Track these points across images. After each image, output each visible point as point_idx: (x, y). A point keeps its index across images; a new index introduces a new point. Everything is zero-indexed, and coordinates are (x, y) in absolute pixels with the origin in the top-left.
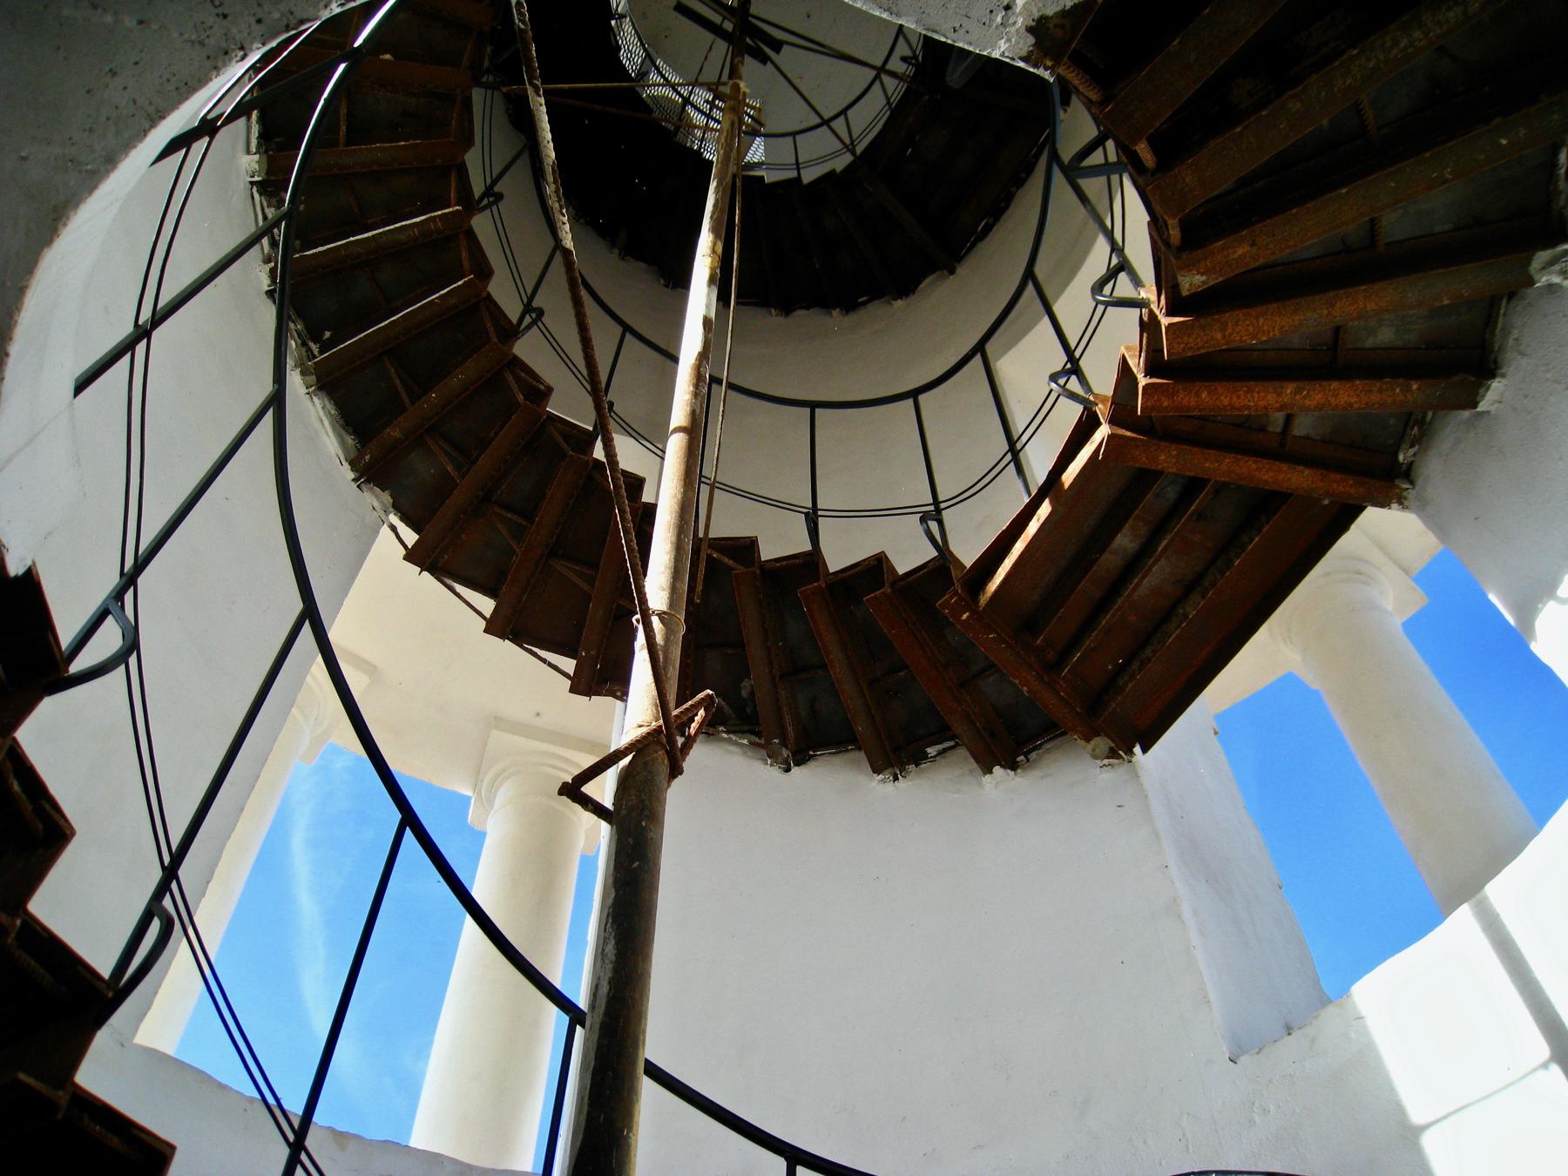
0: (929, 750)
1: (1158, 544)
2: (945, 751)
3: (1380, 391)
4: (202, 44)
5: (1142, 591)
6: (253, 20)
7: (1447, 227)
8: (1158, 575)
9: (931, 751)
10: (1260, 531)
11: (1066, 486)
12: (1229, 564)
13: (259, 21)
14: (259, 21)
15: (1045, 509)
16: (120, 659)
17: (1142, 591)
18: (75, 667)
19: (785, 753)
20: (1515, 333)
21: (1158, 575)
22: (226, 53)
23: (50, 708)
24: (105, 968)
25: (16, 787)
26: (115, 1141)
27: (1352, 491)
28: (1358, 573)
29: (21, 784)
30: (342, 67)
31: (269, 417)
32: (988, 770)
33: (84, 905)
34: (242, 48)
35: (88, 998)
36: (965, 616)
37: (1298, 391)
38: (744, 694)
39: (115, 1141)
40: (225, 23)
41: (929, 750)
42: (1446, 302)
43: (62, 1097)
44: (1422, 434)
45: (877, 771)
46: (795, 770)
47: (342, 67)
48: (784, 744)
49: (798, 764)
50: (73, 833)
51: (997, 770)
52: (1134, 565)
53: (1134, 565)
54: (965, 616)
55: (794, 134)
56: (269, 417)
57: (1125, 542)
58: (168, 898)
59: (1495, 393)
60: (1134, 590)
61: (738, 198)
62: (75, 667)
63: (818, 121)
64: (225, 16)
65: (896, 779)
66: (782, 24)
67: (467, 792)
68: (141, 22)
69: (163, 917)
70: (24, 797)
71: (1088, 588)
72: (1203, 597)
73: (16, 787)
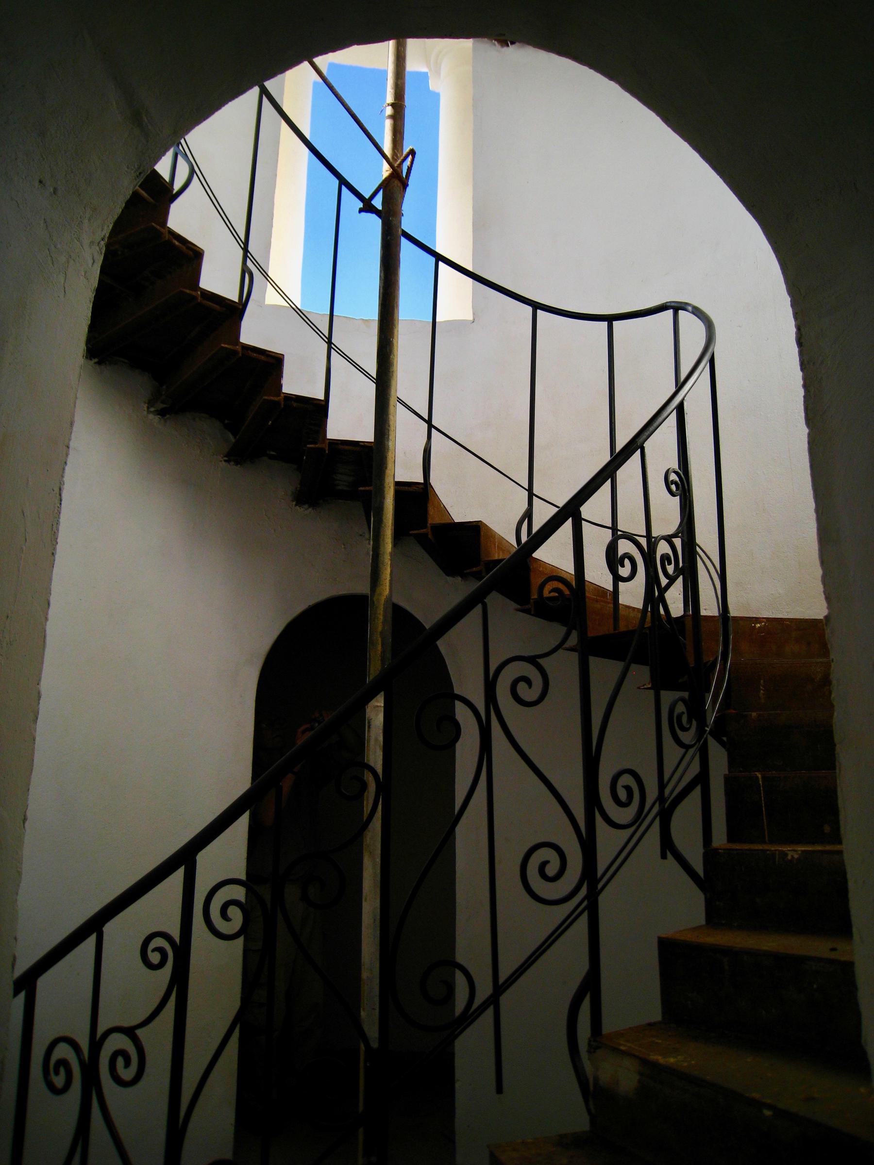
11: (382, 693)
16: (192, 172)
18: (177, 186)
23: (176, 209)
24: (235, 298)
25: (177, 243)
26: (263, 358)
31: (265, 99)
33: (218, 278)
35: (233, 312)
39: (263, 358)
43: (238, 348)
50: (203, 251)
55: (610, 319)
56: (265, 99)
61: (380, 807)
62: (177, 186)
67: (424, 69)
69: (250, 272)
73: (177, 243)
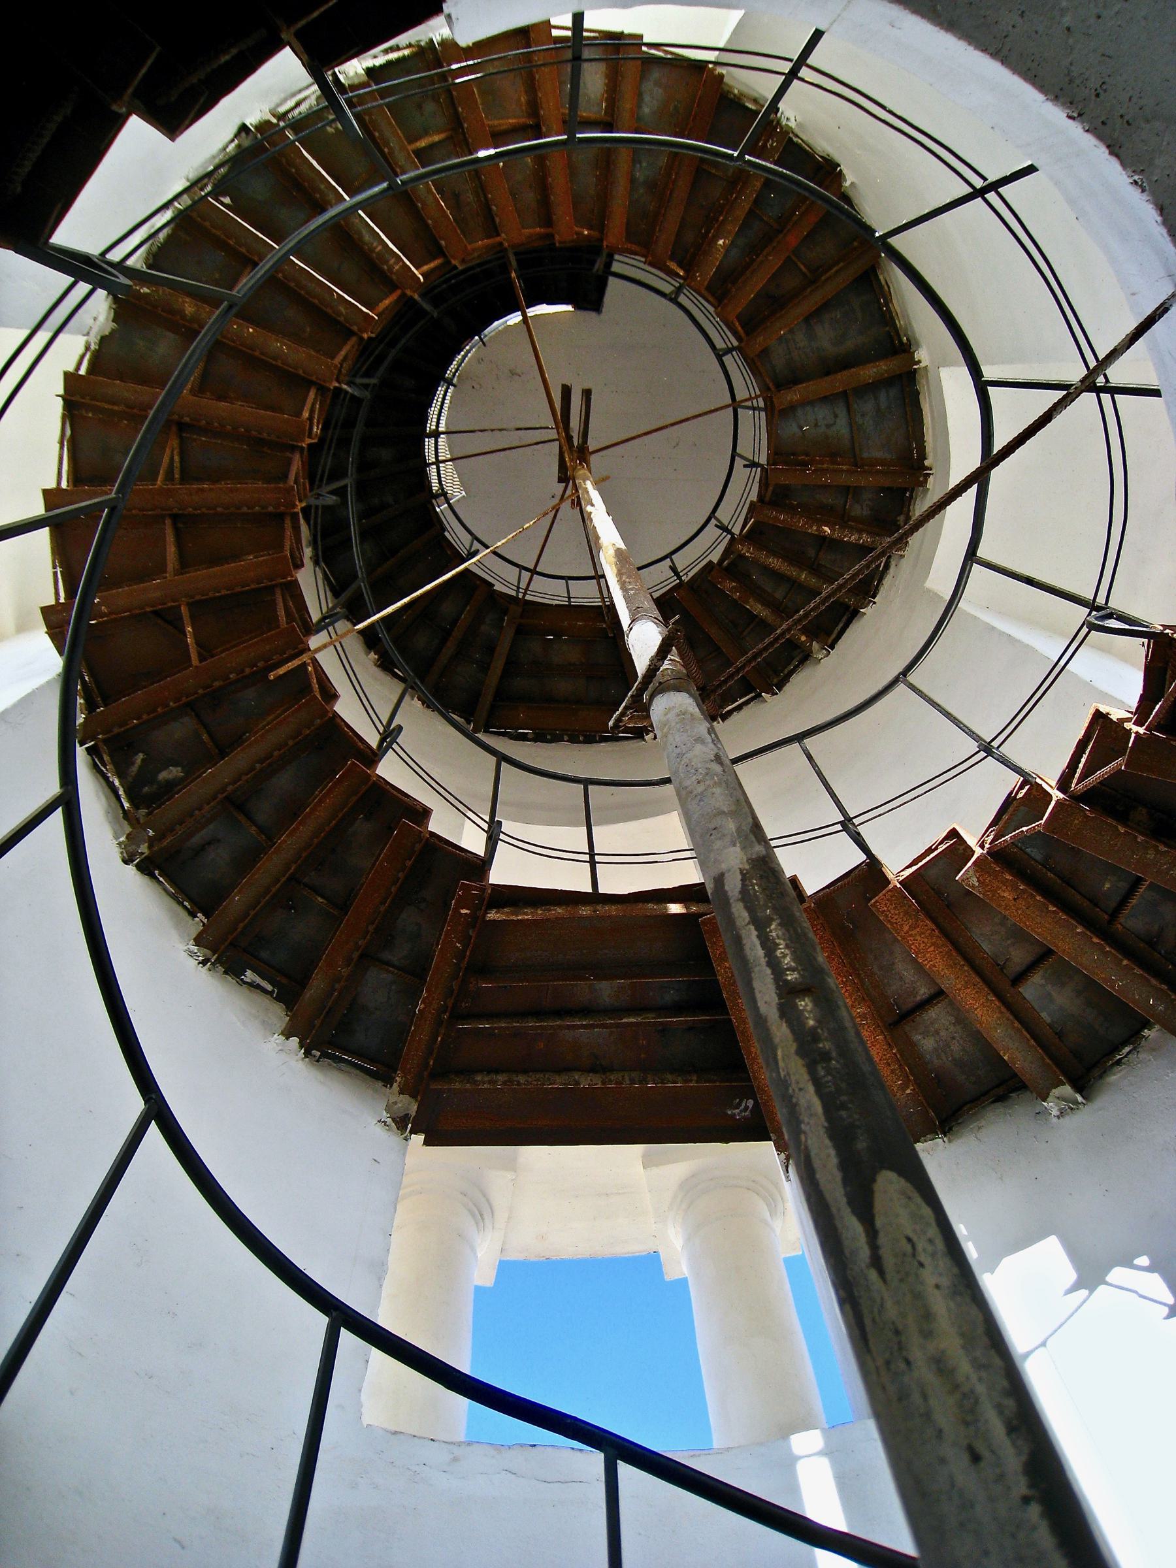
0: (249, 973)
1: (629, 1016)
2: (258, 987)
3: (892, 1072)
4: (1071, 82)
5: (569, 1035)
6: (1103, 118)
7: (1048, 1020)
9: (249, 976)
10: (686, 1081)
13: (1103, 123)
14: (1103, 123)
17: (569, 1035)
19: (144, 848)
20: (983, 1122)
21: (585, 1034)
22: (1071, 103)
25: (224, 59)
28: (481, 1215)
29: (227, 63)
32: (287, 1034)
34: (1080, 115)
38: (163, 775)
40: (1093, 97)
41: (249, 973)
42: (1006, 1058)
45: (198, 941)
46: (131, 869)
48: (152, 842)
49: (139, 867)
51: (295, 1040)
57: (606, 991)
58: (130, 263)
60: (569, 1027)
63: (593, 574)
64: (1097, 95)
65: (204, 963)
68: (1068, 29)
70: (215, 66)
72: (603, 1083)
73: (224, 59)
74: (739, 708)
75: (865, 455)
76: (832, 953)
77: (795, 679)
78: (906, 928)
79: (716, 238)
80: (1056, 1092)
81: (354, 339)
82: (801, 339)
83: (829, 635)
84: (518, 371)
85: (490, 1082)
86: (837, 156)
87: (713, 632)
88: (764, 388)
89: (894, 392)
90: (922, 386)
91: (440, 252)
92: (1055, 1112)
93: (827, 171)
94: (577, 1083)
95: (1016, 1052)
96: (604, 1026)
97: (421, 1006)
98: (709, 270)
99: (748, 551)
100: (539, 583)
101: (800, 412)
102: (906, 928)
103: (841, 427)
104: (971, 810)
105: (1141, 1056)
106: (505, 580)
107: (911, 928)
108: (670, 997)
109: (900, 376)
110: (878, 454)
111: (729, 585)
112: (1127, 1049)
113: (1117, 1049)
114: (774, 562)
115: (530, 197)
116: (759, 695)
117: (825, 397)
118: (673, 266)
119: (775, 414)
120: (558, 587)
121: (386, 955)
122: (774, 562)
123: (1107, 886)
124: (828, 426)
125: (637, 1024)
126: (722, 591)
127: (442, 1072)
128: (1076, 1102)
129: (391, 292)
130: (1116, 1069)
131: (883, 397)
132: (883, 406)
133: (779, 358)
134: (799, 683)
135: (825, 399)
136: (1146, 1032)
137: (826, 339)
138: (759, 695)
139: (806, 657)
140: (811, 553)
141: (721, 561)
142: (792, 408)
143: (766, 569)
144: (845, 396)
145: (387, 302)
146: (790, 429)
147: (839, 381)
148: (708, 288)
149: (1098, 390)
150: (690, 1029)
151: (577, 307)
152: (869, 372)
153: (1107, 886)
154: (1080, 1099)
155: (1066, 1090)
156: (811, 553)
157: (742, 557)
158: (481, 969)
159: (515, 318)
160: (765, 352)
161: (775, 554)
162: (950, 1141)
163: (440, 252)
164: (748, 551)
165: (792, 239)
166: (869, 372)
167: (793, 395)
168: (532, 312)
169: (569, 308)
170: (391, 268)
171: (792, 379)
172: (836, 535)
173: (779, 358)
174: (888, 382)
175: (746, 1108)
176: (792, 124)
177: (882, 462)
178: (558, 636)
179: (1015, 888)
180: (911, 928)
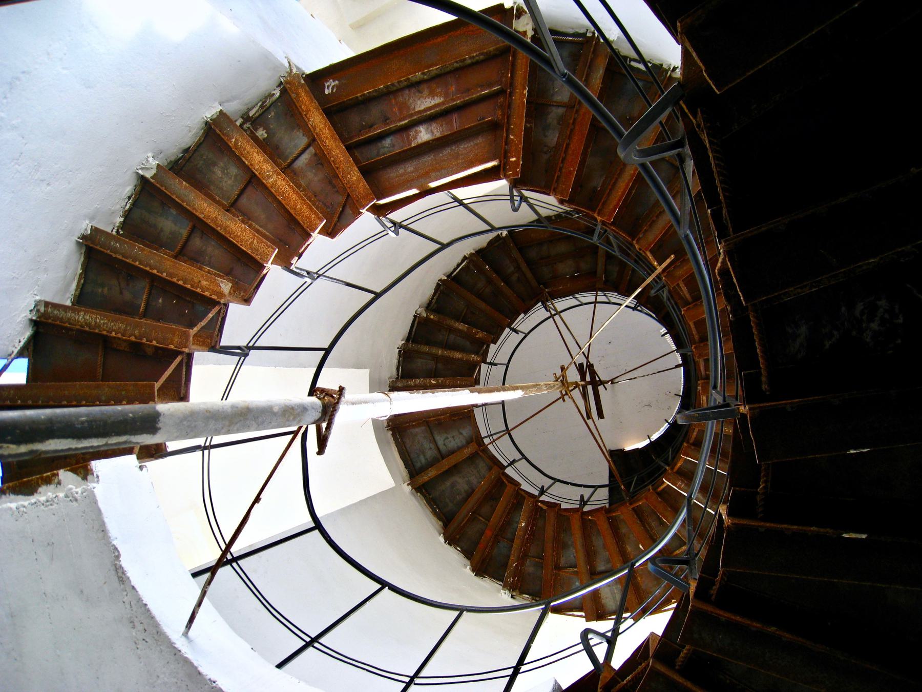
3: (245, 149)
8: (425, 103)
12: (387, 87)
15: (433, 185)
17: (438, 100)
21: (425, 103)
27: (303, 94)
30: (844, 535)
31: (207, 575)
36: (513, 159)
37: (269, 177)
44: (266, 98)
47: (864, 536)
52: (428, 119)
53: (428, 119)
54: (513, 159)
57: (424, 135)
59: (210, 113)
66: (282, 451)
71: (456, 123)
74: (458, 265)
75: (423, 428)
76: (295, 209)
77: (432, 291)
78: (255, 241)
79: (527, 526)
80: (153, 172)
81: (691, 441)
82: (474, 480)
83: (419, 323)
84: (647, 408)
85: (473, 57)
86: (478, 580)
87: (482, 305)
88: (485, 450)
89: (418, 465)
90: (404, 472)
91: (659, 494)
92: (151, 159)
93: (480, 570)
94: (423, 74)
95: (180, 188)
96: (420, 112)
97: (526, 92)
98: (527, 506)
99: (474, 358)
100: (593, 299)
101: (464, 442)
102: (255, 241)
103: (440, 439)
104: (319, 249)
105: (118, 206)
106: (614, 297)
107: (252, 242)
108: (387, 142)
109: (417, 474)
110: (417, 430)
111: (480, 335)
112: (128, 207)
113: (133, 204)
114: (458, 355)
115: (624, 530)
116: (448, 276)
117: (453, 453)
118: (544, 507)
119: (477, 439)
120: (584, 300)
121: (561, 111)
122: (458, 355)
123: (160, 301)
124: (447, 438)
125: (400, 121)
126: (483, 331)
127: (504, 52)
128: (142, 169)
129: (679, 468)
130: (129, 194)
131: (423, 461)
132: (422, 457)
133: (482, 465)
134: (428, 291)
135: (452, 452)
136: (122, 219)
137: (461, 483)
138: (448, 276)
139: (429, 307)
140: (440, 366)
141: (488, 346)
142: (469, 442)
143: (461, 350)
144: (443, 456)
145: (679, 465)
146: (466, 432)
147: (446, 464)
148: (524, 498)
149: (229, 562)
150: (371, 126)
151: (622, 451)
152: (432, 473)
153: (160, 301)
154: (140, 172)
155: (148, 175)
156: (440, 366)
157: (477, 353)
158: (494, 127)
159: (655, 437)
160: (490, 469)
161: (459, 359)
162: (78, 243)
163: (659, 494)
164: (474, 358)
165: (488, 533)
166: (432, 473)
167: (467, 451)
168: (647, 442)
169: (628, 448)
170: (683, 482)
171: (472, 458)
172: (428, 380)
173: (482, 465)
174: (424, 469)
175: (328, 87)
176: (502, 592)
177: (414, 426)
178: (573, 277)
179: (202, 288)
180: (252, 242)
